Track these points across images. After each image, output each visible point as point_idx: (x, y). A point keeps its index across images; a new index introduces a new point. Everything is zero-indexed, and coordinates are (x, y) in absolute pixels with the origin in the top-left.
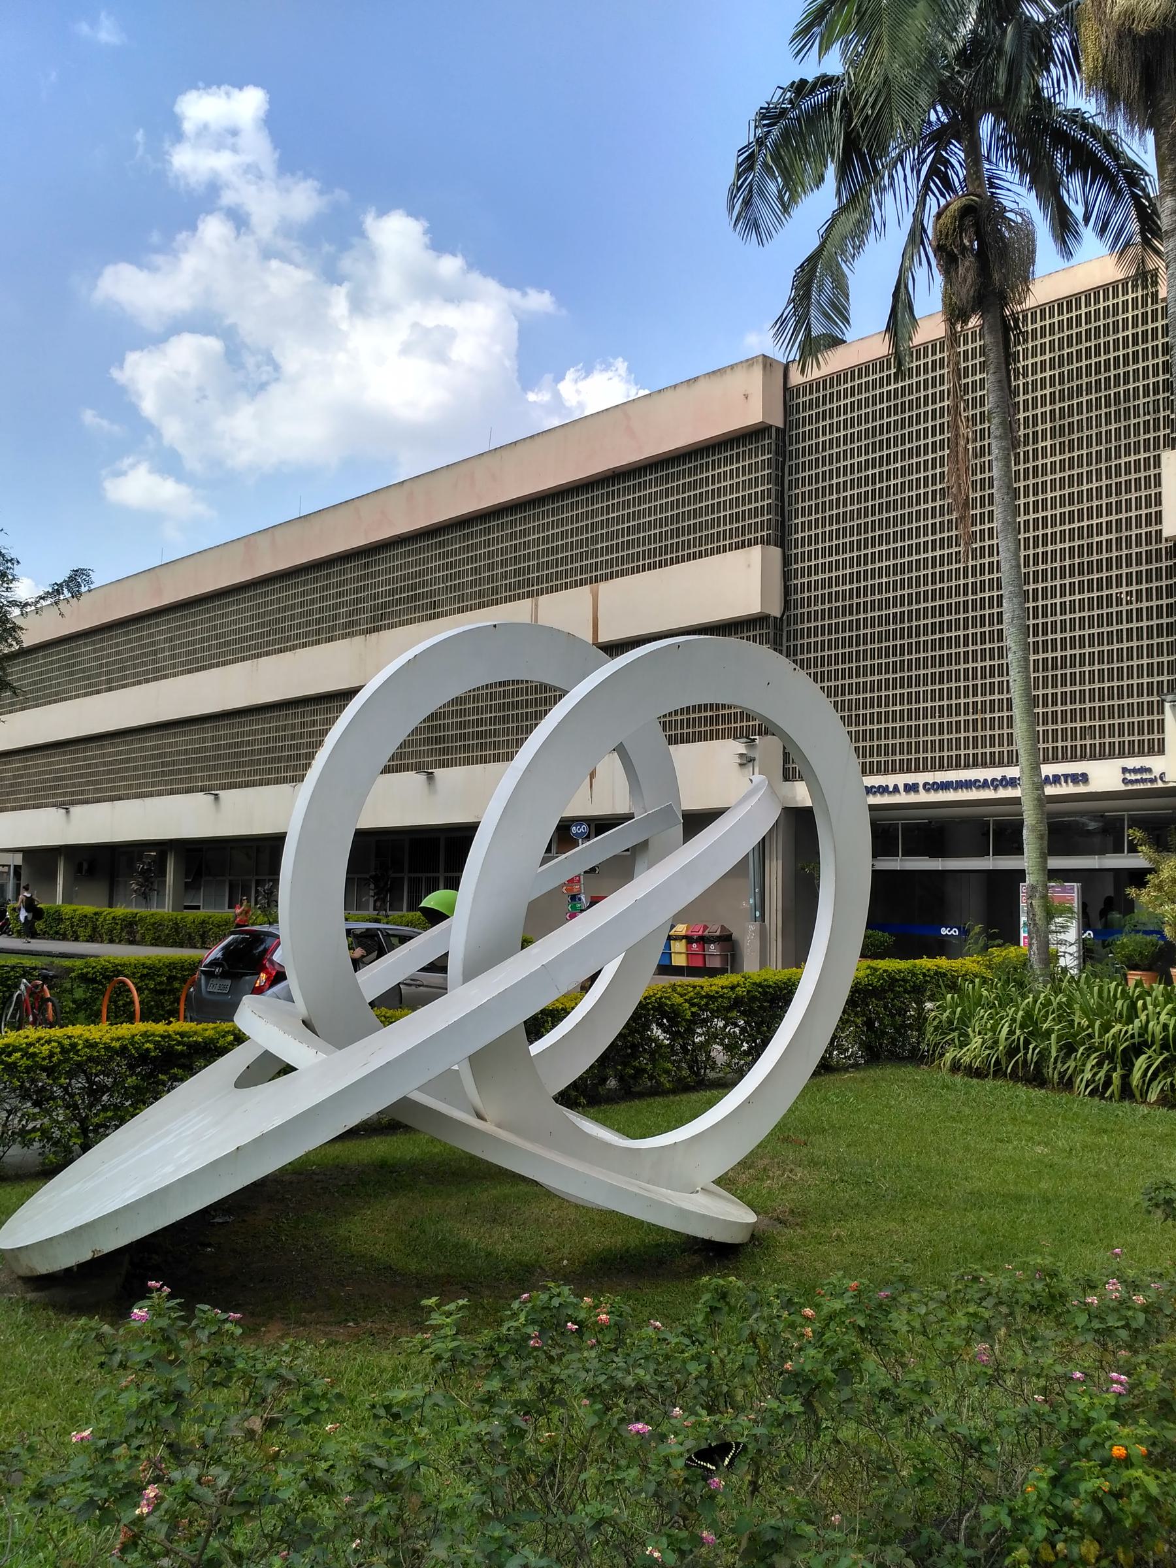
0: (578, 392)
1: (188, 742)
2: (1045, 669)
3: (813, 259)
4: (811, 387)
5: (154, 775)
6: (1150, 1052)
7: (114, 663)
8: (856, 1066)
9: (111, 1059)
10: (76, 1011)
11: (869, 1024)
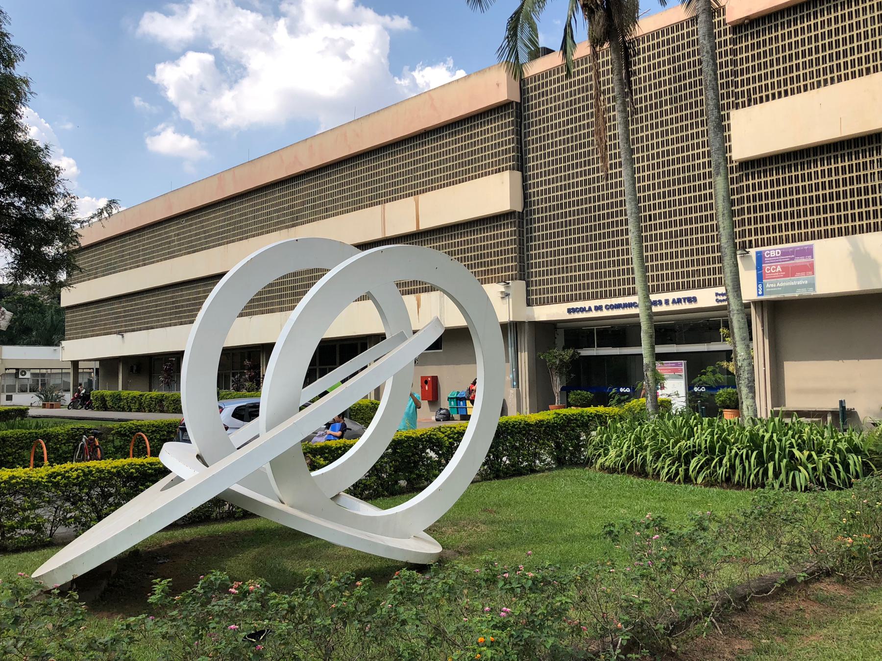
0: (423, 76)
1: (190, 294)
2: (671, 237)
3: (517, 13)
4: (536, 78)
5: (171, 314)
6: (699, 456)
7: (147, 249)
8: (550, 469)
9: (111, 479)
10: (116, 452)
11: (558, 446)
